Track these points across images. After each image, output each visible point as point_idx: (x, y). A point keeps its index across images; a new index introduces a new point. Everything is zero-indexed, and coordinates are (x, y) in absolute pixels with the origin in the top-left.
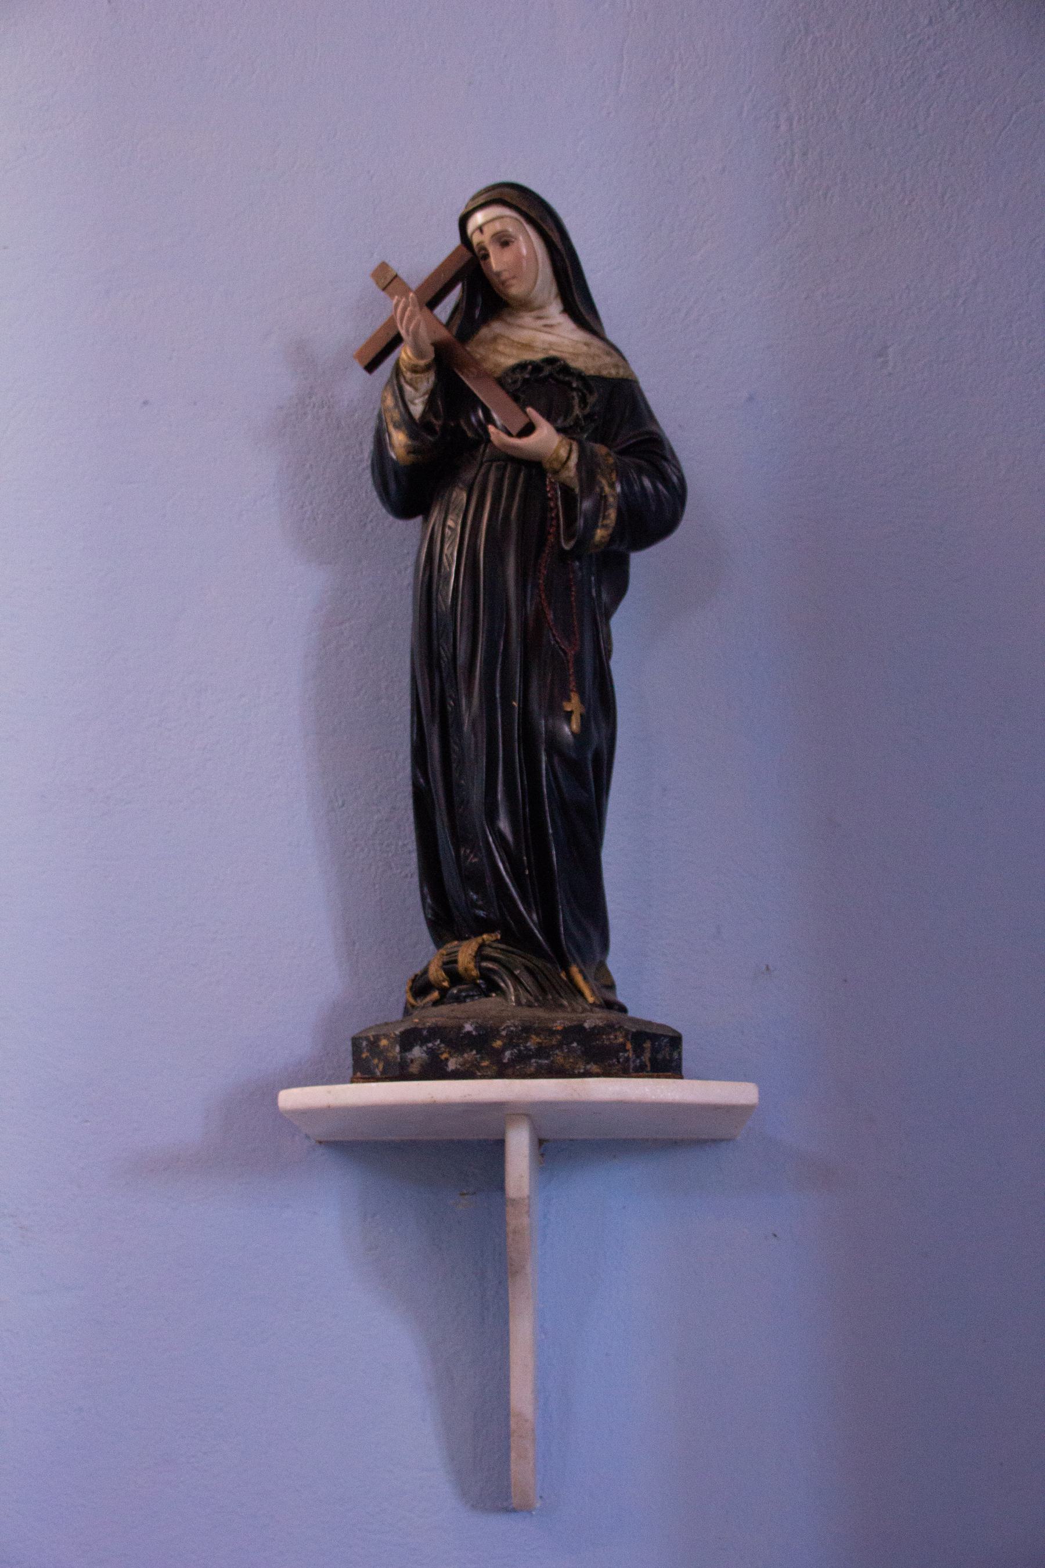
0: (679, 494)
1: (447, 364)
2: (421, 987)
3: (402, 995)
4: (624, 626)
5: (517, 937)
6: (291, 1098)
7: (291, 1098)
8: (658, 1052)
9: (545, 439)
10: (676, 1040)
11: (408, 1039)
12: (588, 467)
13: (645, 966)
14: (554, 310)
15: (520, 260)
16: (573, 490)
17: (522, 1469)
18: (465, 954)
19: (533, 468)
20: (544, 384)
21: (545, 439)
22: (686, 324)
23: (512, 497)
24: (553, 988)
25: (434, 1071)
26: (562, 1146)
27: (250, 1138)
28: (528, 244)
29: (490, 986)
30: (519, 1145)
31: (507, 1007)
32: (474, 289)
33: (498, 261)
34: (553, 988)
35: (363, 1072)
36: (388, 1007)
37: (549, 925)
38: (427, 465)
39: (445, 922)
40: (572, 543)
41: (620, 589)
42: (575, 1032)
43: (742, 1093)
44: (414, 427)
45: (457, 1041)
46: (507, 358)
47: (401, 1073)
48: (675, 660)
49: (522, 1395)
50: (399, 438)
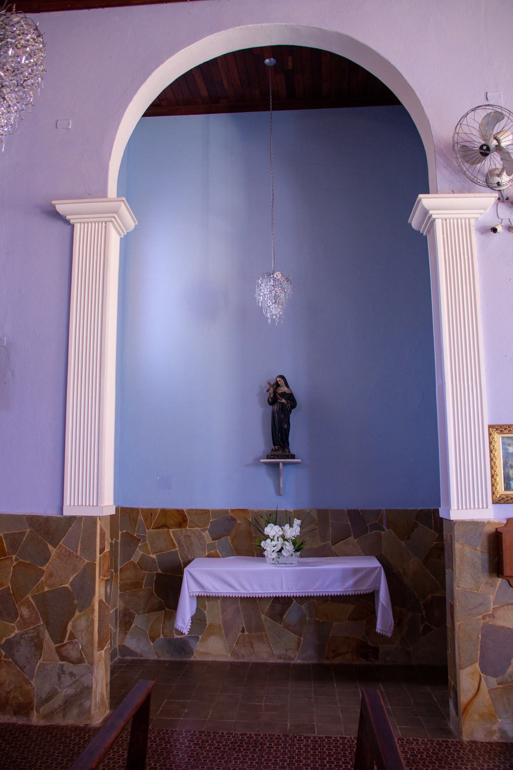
0: (296, 404)
1: (275, 392)
2: (272, 450)
3: (271, 451)
4: (291, 416)
5: (281, 446)
6: (261, 460)
7: (261, 460)
8: (293, 457)
9: (283, 401)
10: (294, 455)
11: (271, 456)
12: (287, 403)
13: (293, 448)
14: (285, 387)
15: (281, 382)
16: (489, 115)
17: (281, 492)
18: (276, 447)
19: (283, 403)
20: (283, 395)
21: (283, 401)
22: (298, 387)
23: (281, 404)
24: (284, 451)
25: (274, 458)
26: (284, 464)
27: (256, 463)
28: (282, 381)
29: (278, 450)
30: (281, 464)
31: (280, 452)
32: (277, 385)
33: (279, 383)
34: (284, 451)
35: (267, 458)
36: (269, 452)
37: (284, 445)
38: (273, 401)
39: (274, 444)
40: (42, 723)
41: (291, 412)
42: (286, 455)
43: (300, 460)
44: (272, 398)
45: (276, 456)
46: (280, 392)
47: (271, 458)
48: (297, 420)
49: (281, 486)
50: (270, 400)
